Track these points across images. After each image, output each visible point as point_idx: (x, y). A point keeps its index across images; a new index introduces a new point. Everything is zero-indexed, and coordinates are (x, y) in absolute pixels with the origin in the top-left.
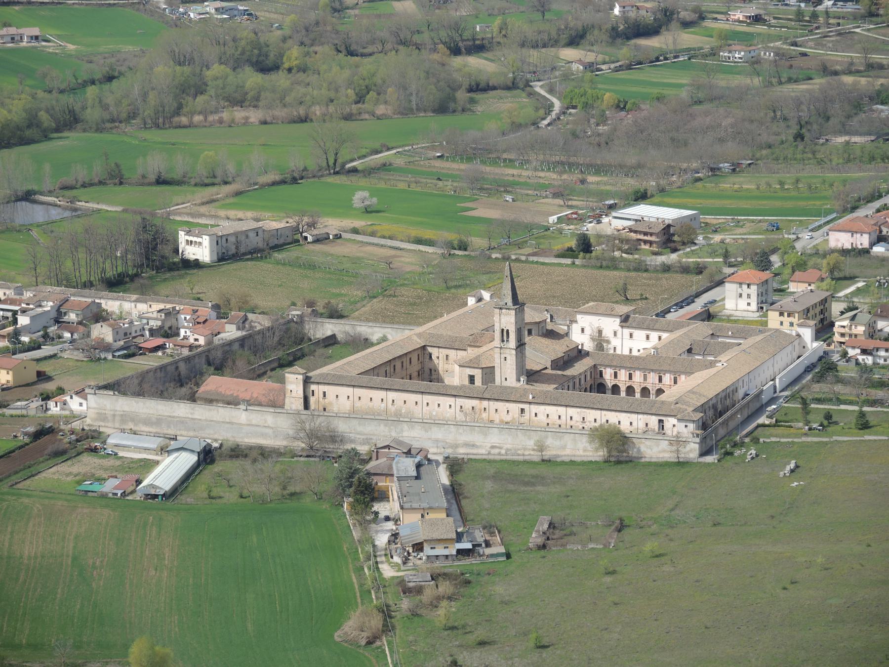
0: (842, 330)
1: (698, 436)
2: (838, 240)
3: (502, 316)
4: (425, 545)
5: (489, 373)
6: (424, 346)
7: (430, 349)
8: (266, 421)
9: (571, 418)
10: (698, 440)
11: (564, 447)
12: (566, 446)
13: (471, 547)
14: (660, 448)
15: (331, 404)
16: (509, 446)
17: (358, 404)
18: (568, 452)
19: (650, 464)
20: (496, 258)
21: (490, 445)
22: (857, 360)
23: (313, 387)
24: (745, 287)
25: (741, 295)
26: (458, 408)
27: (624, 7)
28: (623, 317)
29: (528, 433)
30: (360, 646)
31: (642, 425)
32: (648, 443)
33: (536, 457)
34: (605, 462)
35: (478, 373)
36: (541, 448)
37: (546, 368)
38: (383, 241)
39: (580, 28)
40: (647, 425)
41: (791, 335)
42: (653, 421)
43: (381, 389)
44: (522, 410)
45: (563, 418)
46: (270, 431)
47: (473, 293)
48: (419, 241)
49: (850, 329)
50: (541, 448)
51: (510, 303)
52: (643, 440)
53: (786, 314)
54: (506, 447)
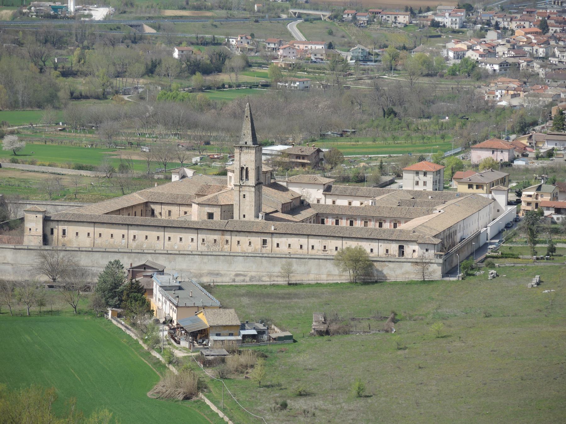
0: (529, 199)
1: (441, 256)
2: (480, 157)
3: (242, 154)
4: (211, 331)
5: (228, 211)
6: (147, 203)
7: (153, 206)
8: (5, 257)
9: (313, 247)
10: (441, 261)
11: (308, 273)
12: (310, 271)
13: (256, 333)
14: (403, 270)
15: (70, 241)
16: (253, 274)
17: (99, 241)
18: (312, 277)
19: (395, 283)
20: (158, 179)
21: (234, 273)
22: (552, 218)
23: (52, 225)
24: (421, 176)
25: (417, 183)
26: (200, 241)
27: (182, 52)
28: (326, 186)
29: (273, 260)
30: (178, 401)
31: (382, 252)
32: (391, 265)
33: (282, 281)
34: (351, 283)
35: (217, 212)
36: (288, 272)
37: (277, 211)
38: (43, 169)
39: (150, 63)
40: (387, 251)
41: (488, 198)
42: (394, 248)
43: (122, 224)
44: (265, 242)
45: (305, 247)
46: (9, 268)
47: (178, 170)
48: (80, 168)
49: (537, 198)
50: (288, 272)
51: (250, 143)
52: (387, 263)
53: (475, 187)
54: (250, 274)
